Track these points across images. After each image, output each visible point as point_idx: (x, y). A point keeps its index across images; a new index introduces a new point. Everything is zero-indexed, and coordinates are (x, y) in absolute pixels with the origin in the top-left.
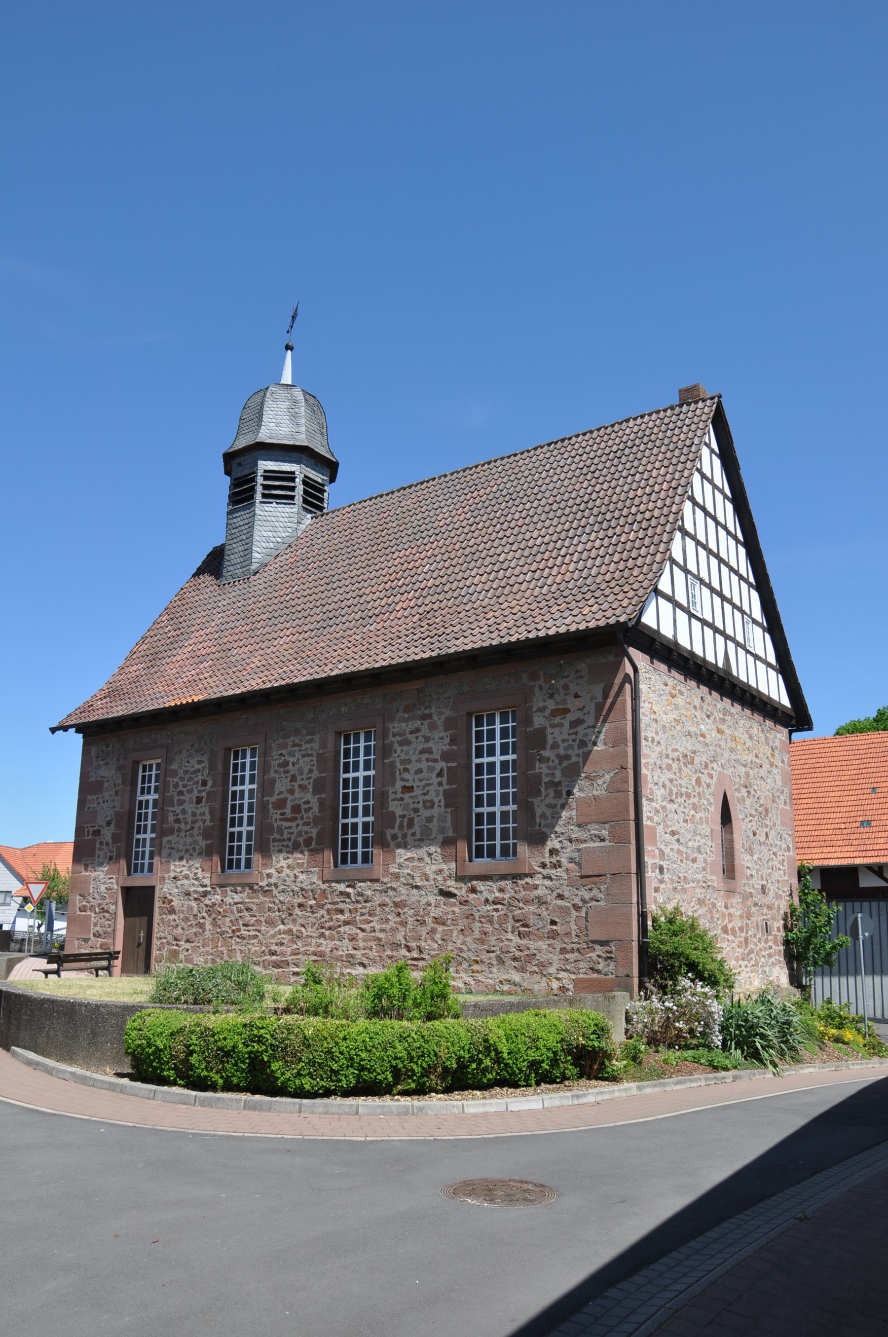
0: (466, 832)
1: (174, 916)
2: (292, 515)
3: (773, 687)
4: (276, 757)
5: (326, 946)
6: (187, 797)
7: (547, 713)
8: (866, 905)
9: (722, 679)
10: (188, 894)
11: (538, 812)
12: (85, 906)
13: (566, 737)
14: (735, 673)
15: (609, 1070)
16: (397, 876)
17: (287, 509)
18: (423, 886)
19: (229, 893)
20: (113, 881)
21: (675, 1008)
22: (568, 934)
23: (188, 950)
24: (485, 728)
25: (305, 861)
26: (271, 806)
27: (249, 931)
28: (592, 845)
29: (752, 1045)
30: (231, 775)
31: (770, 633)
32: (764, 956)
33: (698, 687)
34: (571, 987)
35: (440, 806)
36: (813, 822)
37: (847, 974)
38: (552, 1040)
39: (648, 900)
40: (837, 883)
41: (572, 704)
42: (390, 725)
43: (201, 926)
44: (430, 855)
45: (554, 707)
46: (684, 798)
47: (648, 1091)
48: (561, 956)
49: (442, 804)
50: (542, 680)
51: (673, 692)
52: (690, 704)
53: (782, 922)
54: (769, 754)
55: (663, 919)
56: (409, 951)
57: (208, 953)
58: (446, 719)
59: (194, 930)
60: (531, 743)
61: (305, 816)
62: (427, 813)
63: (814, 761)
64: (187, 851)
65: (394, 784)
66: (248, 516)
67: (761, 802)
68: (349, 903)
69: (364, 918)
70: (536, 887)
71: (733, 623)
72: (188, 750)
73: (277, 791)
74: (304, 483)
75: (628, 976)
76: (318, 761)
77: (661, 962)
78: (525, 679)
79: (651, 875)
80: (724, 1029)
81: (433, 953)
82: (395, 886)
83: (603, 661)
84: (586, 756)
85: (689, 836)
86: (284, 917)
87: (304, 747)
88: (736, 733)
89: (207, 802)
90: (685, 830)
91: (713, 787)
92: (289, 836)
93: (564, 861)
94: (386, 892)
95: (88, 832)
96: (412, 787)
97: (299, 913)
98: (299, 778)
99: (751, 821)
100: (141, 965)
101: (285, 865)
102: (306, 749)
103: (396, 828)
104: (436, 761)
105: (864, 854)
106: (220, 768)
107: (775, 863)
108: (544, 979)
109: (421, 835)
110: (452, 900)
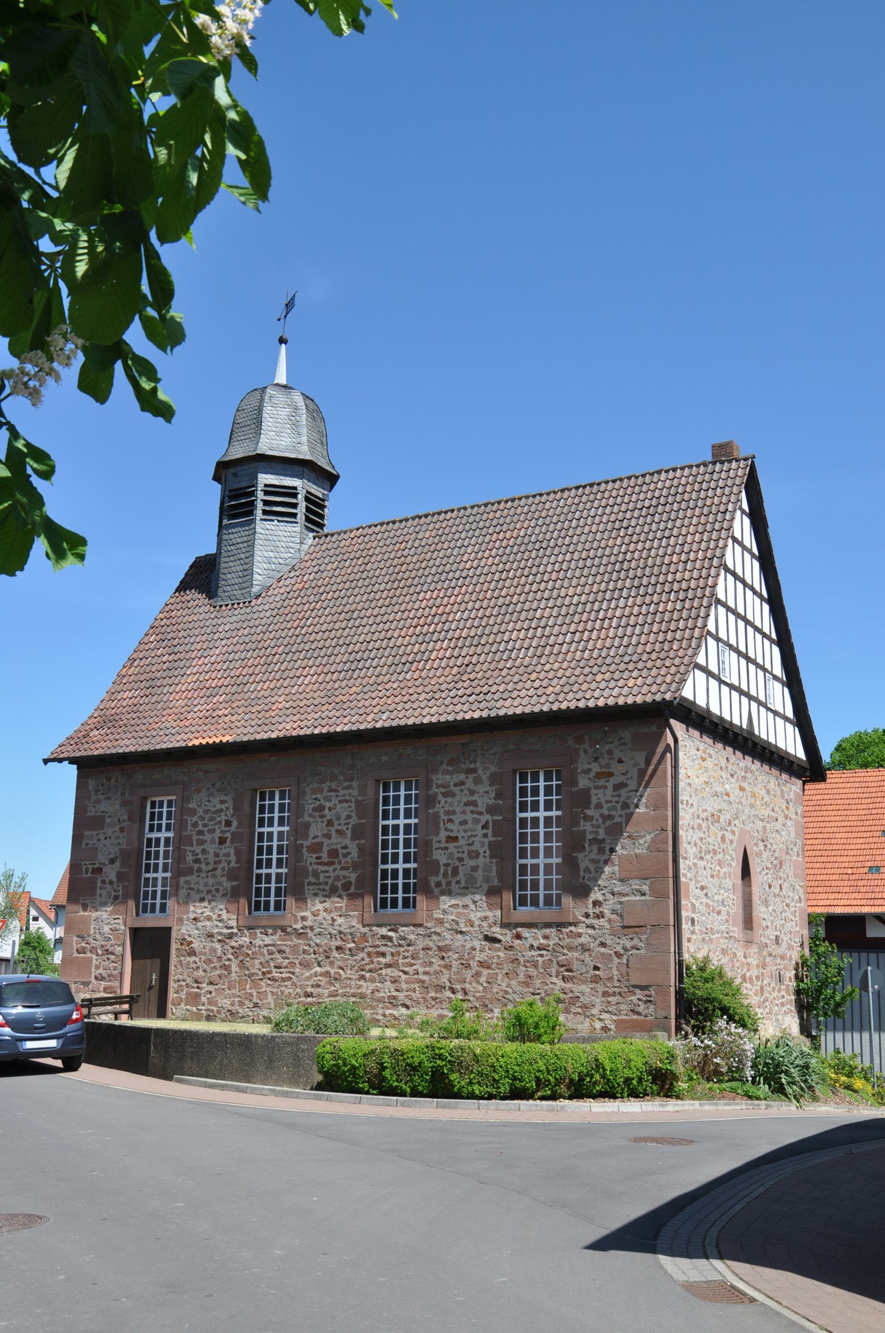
0: (506, 881)
1: (194, 958)
2: (294, 534)
3: (790, 742)
4: (310, 801)
5: (367, 988)
6: (208, 837)
7: (592, 775)
8: (873, 956)
9: (746, 739)
10: (211, 936)
11: (582, 866)
12: (83, 948)
13: (609, 798)
14: (757, 733)
15: (676, 1089)
16: (441, 922)
17: (289, 528)
18: (468, 932)
19: (259, 935)
20: (120, 921)
21: (714, 1045)
22: (610, 979)
23: (211, 993)
24: (529, 785)
25: (344, 905)
26: (305, 849)
27: (281, 973)
28: (633, 898)
29: (778, 1081)
30: (257, 816)
31: (788, 687)
32: (777, 1005)
33: (725, 749)
34: (613, 1027)
35: (485, 857)
36: (818, 865)
37: (852, 1029)
38: (638, 1062)
39: (684, 950)
40: (841, 932)
41: (615, 768)
42: (434, 777)
43: (227, 968)
44: (475, 902)
45: (598, 770)
46: (711, 854)
47: (706, 1107)
48: (604, 999)
49: (487, 854)
50: (587, 744)
51: (704, 755)
52: (717, 765)
53: (794, 972)
54: (784, 807)
55: (694, 967)
56: (454, 993)
57: (234, 996)
58: (492, 775)
59: (218, 972)
60: (575, 802)
61: (343, 861)
62: (472, 863)
63: (819, 797)
64: (209, 892)
65: (438, 834)
66: (247, 533)
67: (777, 855)
68: (391, 947)
69: (406, 961)
70: (580, 935)
71: (756, 683)
72: (208, 789)
73: (311, 835)
74: (307, 499)
75: (666, 1018)
76: (357, 807)
77: (696, 1007)
78: (570, 742)
79: (686, 926)
80: (754, 1066)
81: (478, 995)
82: (439, 931)
83: (646, 730)
84: (629, 817)
85: (715, 890)
86: (320, 959)
87: (341, 793)
88: (755, 789)
89: (232, 843)
90: (712, 884)
91: (735, 843)
92: (326, 880)
93: (607, 912)
94: (429, 936)
95: (87, 870)
96: (457, 837)
97: (337, 956)
98: (336, 823)
99: (767, 874)
100: (154, 1009)
101: (321, 908)
102: (344, 795)
103: (441, 876)
104: (481, 813)
105: (872, 902)
106: (247, 809)
107: (788, 914)
108: (587, 1020)
109: (466, 882)
110: (497, 945)
